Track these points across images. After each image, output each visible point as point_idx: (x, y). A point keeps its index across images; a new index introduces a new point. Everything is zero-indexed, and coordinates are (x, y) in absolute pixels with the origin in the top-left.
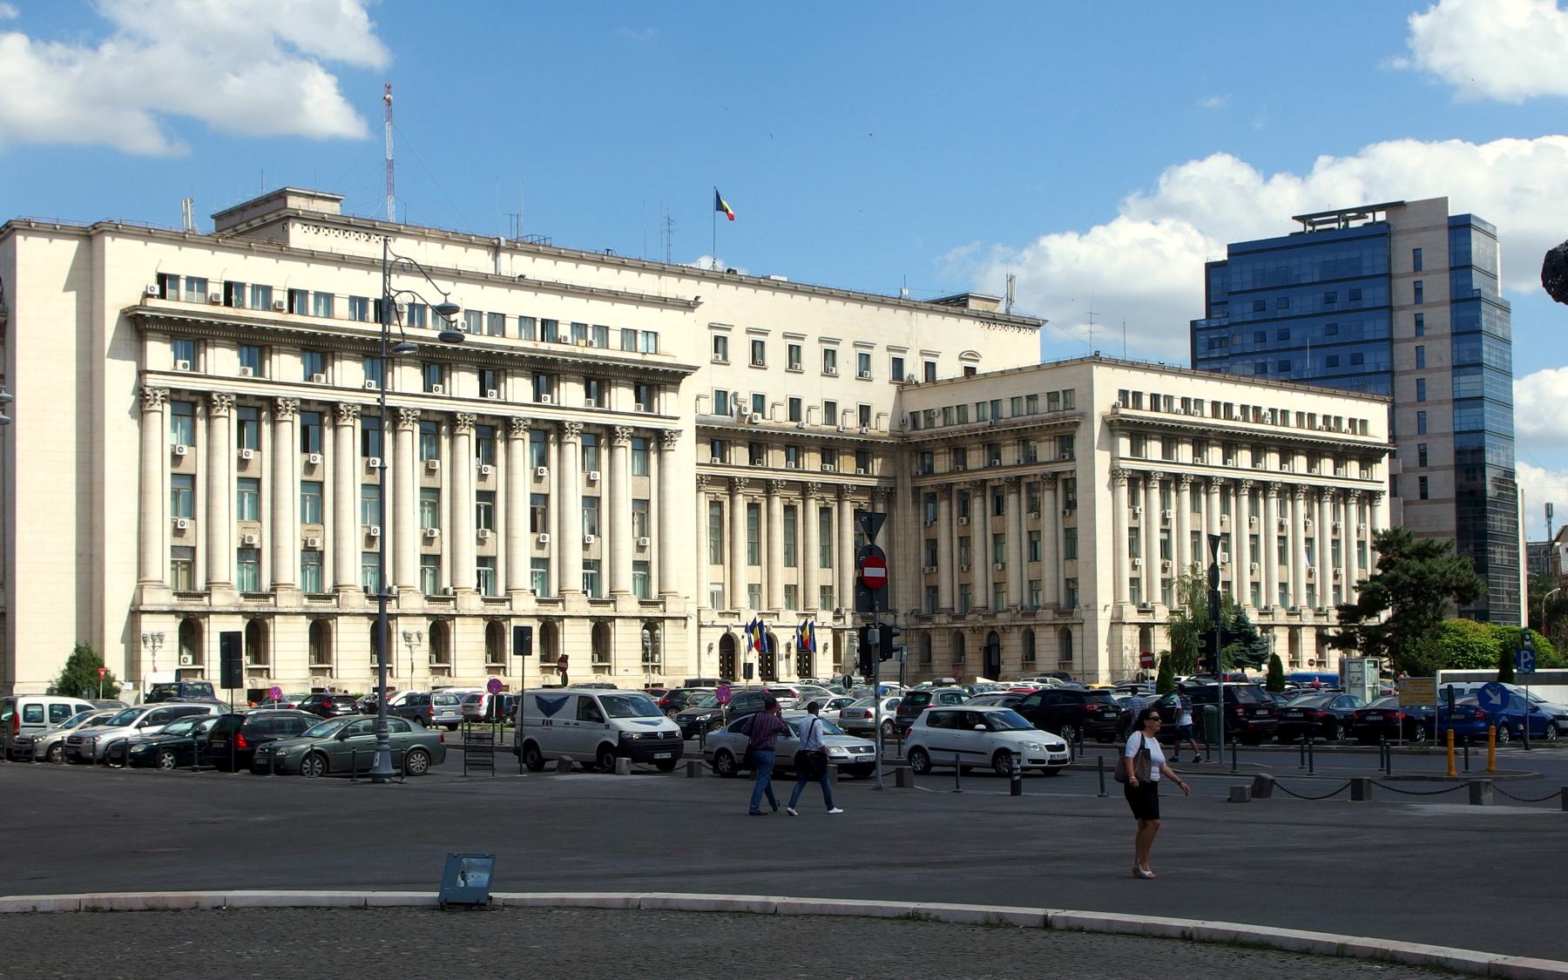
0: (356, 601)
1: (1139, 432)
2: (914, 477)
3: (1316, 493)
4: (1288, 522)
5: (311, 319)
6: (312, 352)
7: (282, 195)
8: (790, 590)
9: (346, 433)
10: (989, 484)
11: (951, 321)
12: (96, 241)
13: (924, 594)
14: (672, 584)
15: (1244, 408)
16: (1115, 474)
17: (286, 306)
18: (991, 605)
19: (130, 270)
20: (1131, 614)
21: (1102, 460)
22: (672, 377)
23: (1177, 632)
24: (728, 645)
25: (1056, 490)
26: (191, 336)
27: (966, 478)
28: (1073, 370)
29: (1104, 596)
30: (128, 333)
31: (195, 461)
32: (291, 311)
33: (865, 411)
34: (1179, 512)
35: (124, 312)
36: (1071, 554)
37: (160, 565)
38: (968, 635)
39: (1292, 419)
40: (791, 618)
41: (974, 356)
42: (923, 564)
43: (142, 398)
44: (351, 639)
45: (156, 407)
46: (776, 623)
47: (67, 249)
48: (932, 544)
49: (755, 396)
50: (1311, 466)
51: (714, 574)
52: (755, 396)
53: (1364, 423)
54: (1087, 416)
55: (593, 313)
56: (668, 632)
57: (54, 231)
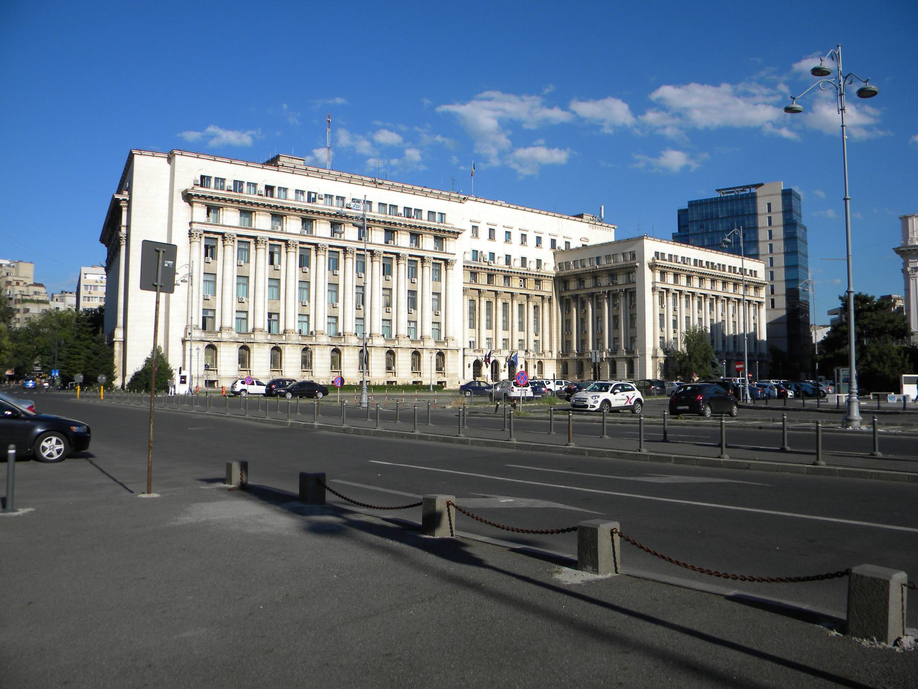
15: (707, 263)
22: (456, 234)
24: (477, 365)
27: (585, 292)
38: (585, 363)
40: (506, 353)
41: (587, 240)
51: (470, 335)
53: (755, 272)
56: (449, 357)
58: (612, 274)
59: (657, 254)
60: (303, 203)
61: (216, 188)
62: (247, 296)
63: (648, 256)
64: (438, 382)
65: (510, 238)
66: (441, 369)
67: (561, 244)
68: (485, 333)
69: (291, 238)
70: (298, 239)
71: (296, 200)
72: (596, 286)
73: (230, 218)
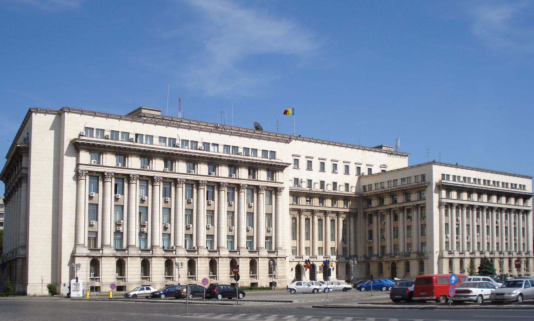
0: (159, 252)
1: (449, 189)
2: (364, 209)
3: (509, 210)
4: (499, 221)
5: (145, 145)
6: (120, 155)
7: (140, 109)
8: (320, 249)
10: (392, 210)
11: (377, 154)
12: (62, 116)
13: (367, 250)
14: (280, 245)
16: (440, 204)
17: (134, 140)
18: (393, 253)
19: (75, 125)
20: (446, 254)
21: (436, 197)
22: (281, 167)
25: (418, 211)
26: (97, 150)
27: (384, 208)
28: (425, 167)
29: (436, 248)
30: (73, 149)
31: (98, 198)
32: (136, 142)
33: (347, 185)
34: (462, 217)
35: (71, 142)
36: (423, 234)
37: (83, 238)
38: (384, 263)
39: (501, 184)
40: (321, 258)
41: (385, 166)
42: (367, 239)
43: (77, 176)
45: (83, 178)
46: (315, 260)
47: (51, 118)
48: (371, 232)
49: (346, 184)
50: (507, 201)
53: (524, 186)
54: (430, 183)
57: (46, 112)
58: (406, 193)
59: (443, 175)
60: (166, 147)
63: (436, 178)
64: (252, 284)
67: (364, 171)
68: (305, 243)
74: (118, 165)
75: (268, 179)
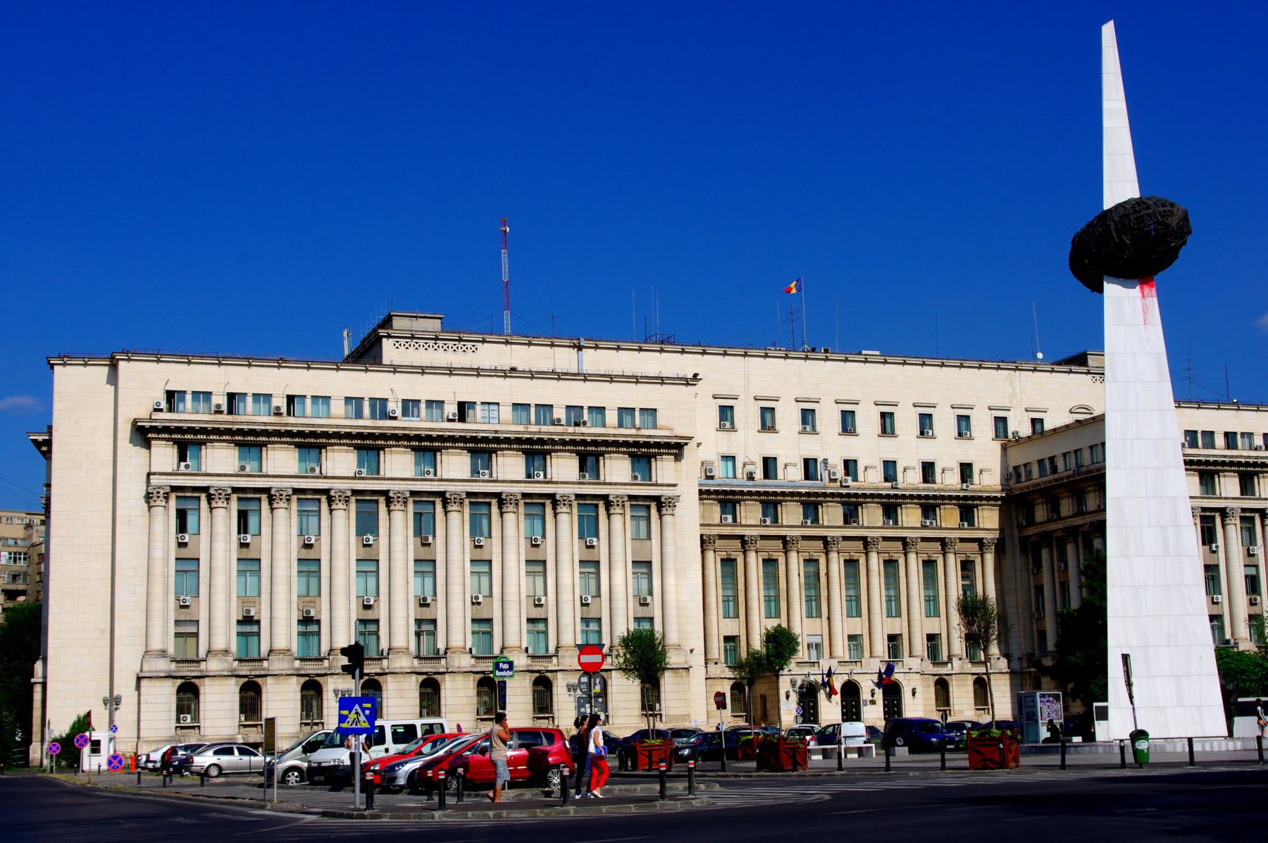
2: (1020, 528)
9: (564, 518)
23: (1056, 688)
27: (1060, 525)
35: (135, 422)
44: (281, 702)
48: (1039, 590)
49: (962, 465)
52: (962, 465)
55: (585, 395)
61: (538, 423)
62: (599, 595)
65: (968, 428)
66: (652, 708)
67: (1020, 425)
69: (559, 490)
70: (518, 489)
71: (621, 425)
72: (1079, 513)
73: (220, 460)
74: (243, 468)
75: (635, 478)
